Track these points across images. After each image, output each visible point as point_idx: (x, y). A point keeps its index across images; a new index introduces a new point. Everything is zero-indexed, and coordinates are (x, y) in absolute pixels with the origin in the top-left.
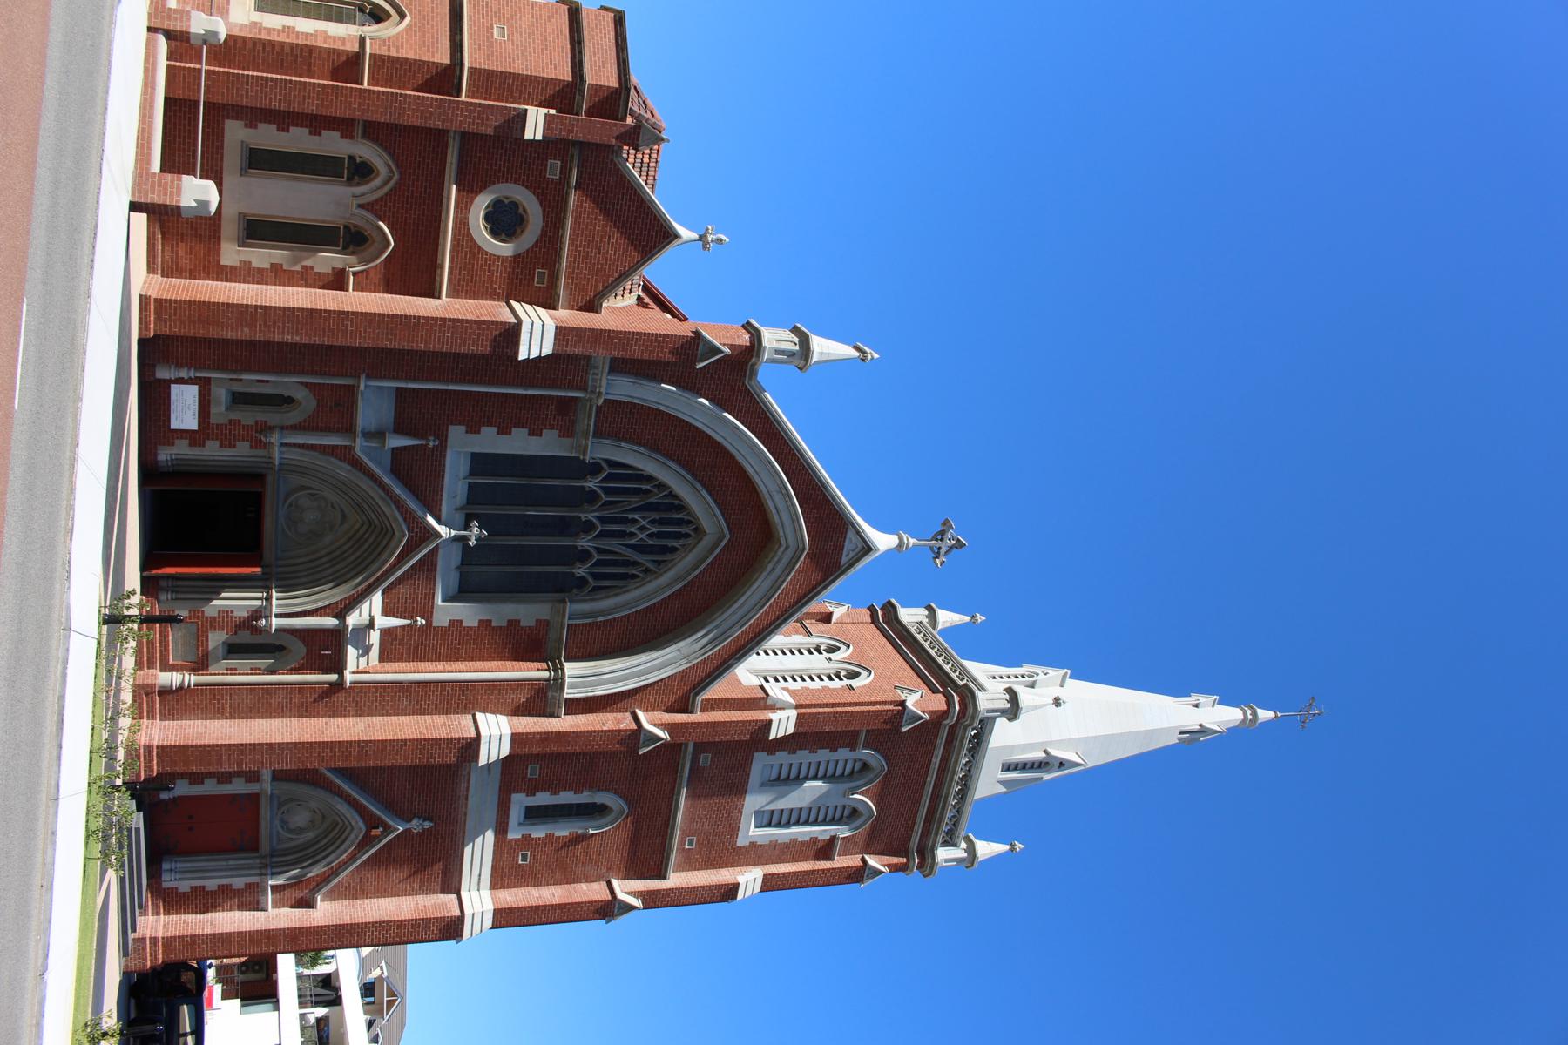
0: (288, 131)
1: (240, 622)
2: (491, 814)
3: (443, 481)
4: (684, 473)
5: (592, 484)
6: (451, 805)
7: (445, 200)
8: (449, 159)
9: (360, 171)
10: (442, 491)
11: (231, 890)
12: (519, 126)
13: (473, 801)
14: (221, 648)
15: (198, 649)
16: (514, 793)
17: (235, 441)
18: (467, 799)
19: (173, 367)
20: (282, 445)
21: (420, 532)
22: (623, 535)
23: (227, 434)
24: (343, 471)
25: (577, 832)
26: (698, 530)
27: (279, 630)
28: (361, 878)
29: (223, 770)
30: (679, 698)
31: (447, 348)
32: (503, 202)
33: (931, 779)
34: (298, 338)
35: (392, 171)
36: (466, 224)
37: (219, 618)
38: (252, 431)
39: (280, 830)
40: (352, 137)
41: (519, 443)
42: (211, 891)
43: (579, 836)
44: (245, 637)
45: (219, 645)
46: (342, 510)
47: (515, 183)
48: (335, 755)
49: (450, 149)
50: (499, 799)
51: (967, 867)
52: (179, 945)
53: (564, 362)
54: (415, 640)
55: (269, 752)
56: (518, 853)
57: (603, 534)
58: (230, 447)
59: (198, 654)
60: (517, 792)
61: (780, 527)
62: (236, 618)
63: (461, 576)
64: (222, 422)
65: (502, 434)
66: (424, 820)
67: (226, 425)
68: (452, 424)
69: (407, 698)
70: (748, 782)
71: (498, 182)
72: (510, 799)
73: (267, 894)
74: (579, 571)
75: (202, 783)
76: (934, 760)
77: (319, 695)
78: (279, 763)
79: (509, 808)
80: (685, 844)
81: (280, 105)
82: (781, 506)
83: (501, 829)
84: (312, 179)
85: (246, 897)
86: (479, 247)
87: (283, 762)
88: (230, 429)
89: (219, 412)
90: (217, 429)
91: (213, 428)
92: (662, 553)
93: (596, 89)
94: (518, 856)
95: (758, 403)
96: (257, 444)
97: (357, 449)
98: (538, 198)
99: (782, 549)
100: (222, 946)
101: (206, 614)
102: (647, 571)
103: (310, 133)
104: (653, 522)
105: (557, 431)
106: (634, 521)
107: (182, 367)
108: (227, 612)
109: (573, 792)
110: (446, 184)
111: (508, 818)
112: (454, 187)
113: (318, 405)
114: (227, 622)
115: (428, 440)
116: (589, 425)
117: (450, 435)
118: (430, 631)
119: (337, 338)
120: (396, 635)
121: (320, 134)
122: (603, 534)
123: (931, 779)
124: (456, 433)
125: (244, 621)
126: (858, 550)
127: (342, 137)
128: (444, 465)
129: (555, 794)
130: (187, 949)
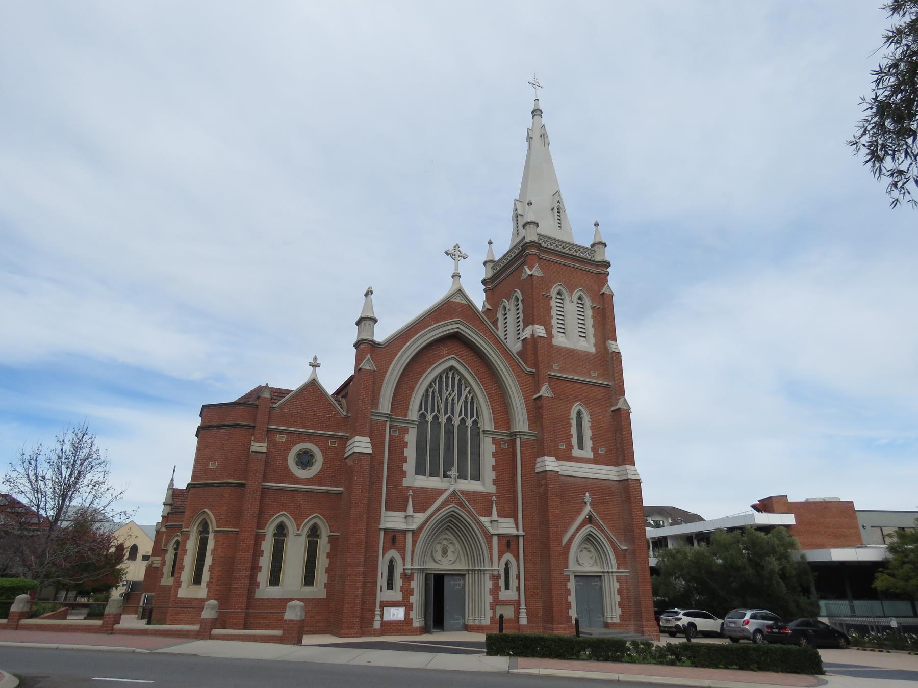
17: (410, 589)
22: (453, 404)
23: (407, 592)
24: (423, 535)
41: (410, 453)
89: (396, 595)
98: (295, 445)
102: (469, 393)
113: (393, 549)
121: (263, 551)
124: (406, 482)
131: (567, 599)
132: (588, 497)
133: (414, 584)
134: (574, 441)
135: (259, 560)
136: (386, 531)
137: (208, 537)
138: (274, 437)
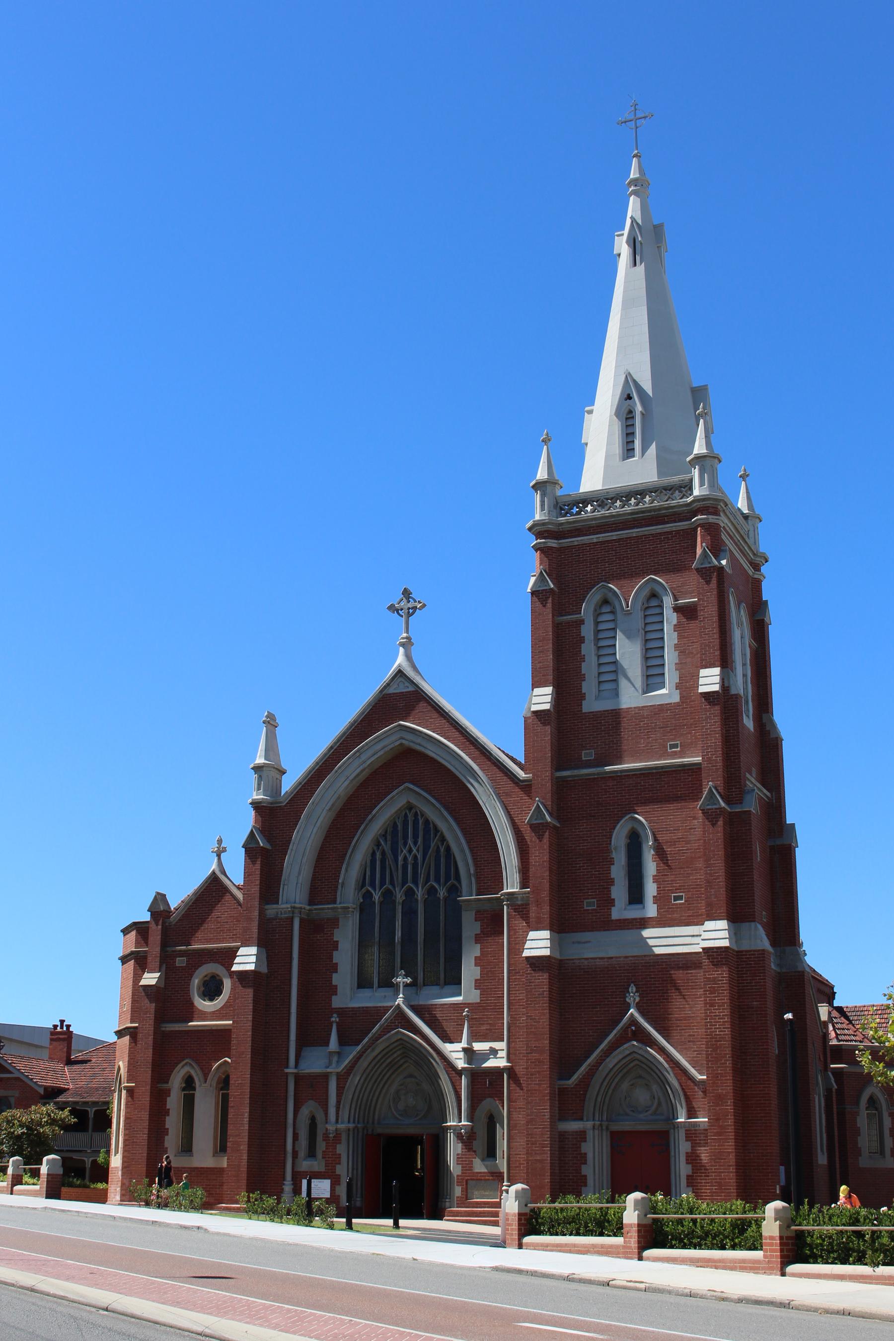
0: (168, 1129)
1: (466, 1149)
2: (627, 935)
3: (370, 1007)
4: (360, 831)
5: (377, 896)
6: (616, 970)
7: (200, 1028)
8: (177, 1029)
9: (189, 1083)
10: (377, 1007)
11: (691, 1153)
12: (149, 989)
13: (612, 952)
14: (486, 1163)
15: (489, 1180)
16: (611, 918)
17: (336, 1155)
18: (612, 958)
19: (282, 1195)
20: (337, 1121)
21: (398, 1020)
23: (332, 1160)
24: (355, 1079)
25: (653, 855)
26: (410, 807)
27: (471, 1118)
28: (689, 1042)
29: (549, 1159)
30: (526, 794)
31: (250, 1017)
32: (204, 991)
33: (614, 535)
34: (246, 1114)
35: (186, 1064)
36: (213, 1013)
37: (462, 1164)
38: (329, 1143)
39: (649, 1112)
40: (169, 1090)
42: (693, 1170)
43: (657, 852)
44: (480, 1143)
45: (484, 1165)
46: (405, 1078)
47: (189, 985)
48: (538, 1072)
49: (172, 1029)
50: (617, 930)
51: (720, 461)
52: (721, 1196)
53: (274, 936)
54: (490, 1015)
55: (534, 1123)
56: (674, 904)
57: (392, 882)
58: (340, 1158)
59: (492, 1179)
60: (611, 915)
61: (386, 749)
62: (462, 1152)
63: (382, 987)
64: (324, 1164)
65: (337, 969)
66: (628, 992)
67: (326, 1161)
68: (331, 1006)
69: (520, 1017)
70: (612, 710)
71: (190, 996)
72: (617, 920)
73: (696, 1122)
74: (441, 894)
75: (586, 1176)
76: (595, 541)
77: (518, 1086)
78: (545, 1115)
79: (625, 920)
80: (675, 752)
81: (145, 1134)
82: (370, 753)
83: (644, 923)
84: (218, 1114)
85: (700, 1140)
86: (226, 1002)
87: (544, 1112)
88: (328, 1158)
89: (317, 1165)
90: (328, 1166)
91: (328, 1170)
92: (430, 829)
93: (137, 944)
94: (677, 904)
95: (297, 792)
96: (337, 1138)
97: (339, 1070)
98: (197, 969)
99: (404, 742)
100: (725, 1159)
101: (460, 1173)
103: (168, 1115)
104: (405, 844)
105: (335, 930)
106: (405, 858)
107: (283, 1189)
108: (459, 1158)
109: (612, 866)
110: (190, 1029)
111: (635, 919)
112: (190, 1024)
113: (312, 1099)
114: (466, 1158)
115: (333, 1022)
116: (328, 909)
117: (338, 1007)
118: (483, 1003)
119: (246, 1089)
120: (487, 1029)
121: (169, 1109)
122: (392, 882)
123: (614, 535)
124: (337, 1002)
125: (465, 1146)
126: (403, 680)
127: (169, 1096)
128: (359, 1008)
129: (614, 882)
130: (725, 1189)
131: (578, 1170)
132: (633, 996)
133: (341, 1149)
134: (619, 891)
135: (165, 1121)
136: (298, 1078)
137: (194, 1094)
138: (189, 961)
